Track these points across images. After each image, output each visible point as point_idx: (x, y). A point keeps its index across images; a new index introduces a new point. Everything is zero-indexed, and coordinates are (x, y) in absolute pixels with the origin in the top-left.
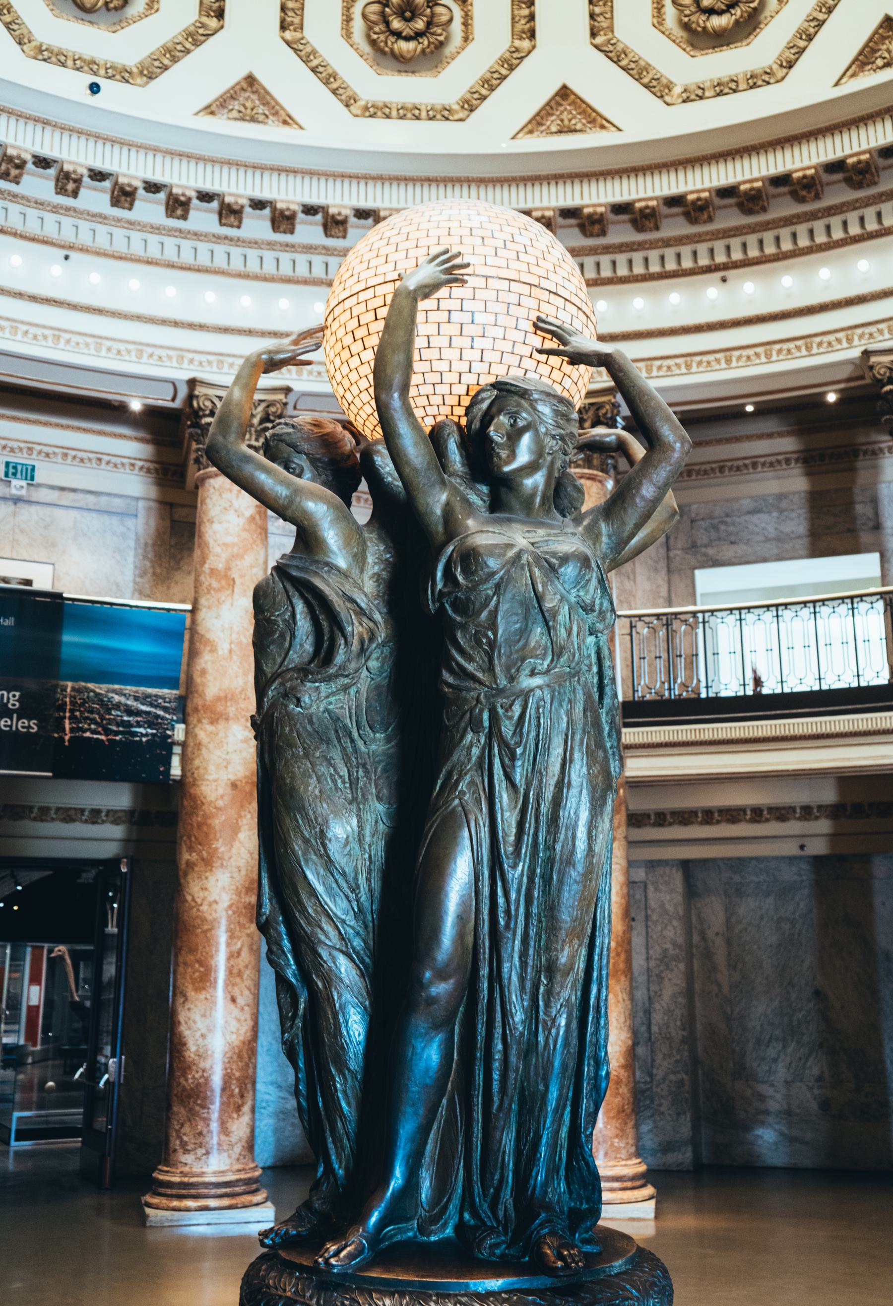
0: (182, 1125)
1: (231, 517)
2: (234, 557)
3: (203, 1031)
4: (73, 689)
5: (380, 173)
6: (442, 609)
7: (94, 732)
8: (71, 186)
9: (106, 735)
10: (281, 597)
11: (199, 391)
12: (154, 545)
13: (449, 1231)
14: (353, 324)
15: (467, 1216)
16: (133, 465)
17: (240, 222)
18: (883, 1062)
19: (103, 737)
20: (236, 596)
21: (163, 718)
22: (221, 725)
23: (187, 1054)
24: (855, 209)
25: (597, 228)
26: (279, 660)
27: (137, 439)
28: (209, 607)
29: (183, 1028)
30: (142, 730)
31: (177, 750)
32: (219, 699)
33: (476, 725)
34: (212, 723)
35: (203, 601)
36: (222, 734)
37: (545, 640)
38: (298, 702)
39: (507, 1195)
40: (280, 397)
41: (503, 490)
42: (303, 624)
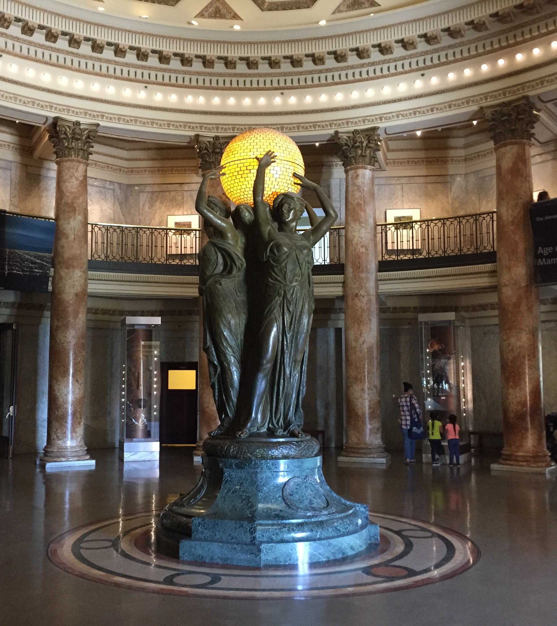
0: (57, 429)
1: (74, 180)
2: (75, 198)
3: (65, 393)
4: (9, 252)
5: (142, 31)
6: (268, 260)
7: (17, 271)
8: (6, 24)
9: (23, 272)
10: (213, 252)
11: (59, 123)
12: (19, 183)
13: (265, 430)
14: (239, 169)
15: (270, 426)
16: (9, 146)
17: (79, 47)
18: (316, 406)
19: (21, 273)
20: (76, 215)
21: (46, 266)
22: (71, 270)
23: (58, 402)
24: (337, 71)
25: (232, 65)
26: (212, 271)
27: (11, 134)
28: (65, 219)
29: (56, 392)
30: (37, 270)
31: (51, 279)
32: (70, 258)
33: (279, 295)
34: (67, 269)
35: (61, 216)
36: (71, 274)
37: (300, 271)
38: (221, 284)
39: (281, 421)
40: (94, 128)
41: (283, 225)
42: (221, 260)
